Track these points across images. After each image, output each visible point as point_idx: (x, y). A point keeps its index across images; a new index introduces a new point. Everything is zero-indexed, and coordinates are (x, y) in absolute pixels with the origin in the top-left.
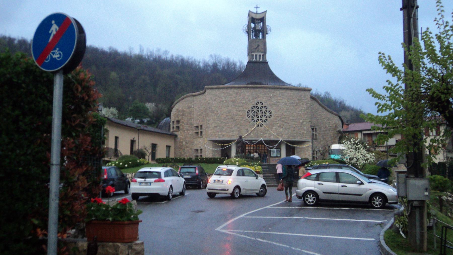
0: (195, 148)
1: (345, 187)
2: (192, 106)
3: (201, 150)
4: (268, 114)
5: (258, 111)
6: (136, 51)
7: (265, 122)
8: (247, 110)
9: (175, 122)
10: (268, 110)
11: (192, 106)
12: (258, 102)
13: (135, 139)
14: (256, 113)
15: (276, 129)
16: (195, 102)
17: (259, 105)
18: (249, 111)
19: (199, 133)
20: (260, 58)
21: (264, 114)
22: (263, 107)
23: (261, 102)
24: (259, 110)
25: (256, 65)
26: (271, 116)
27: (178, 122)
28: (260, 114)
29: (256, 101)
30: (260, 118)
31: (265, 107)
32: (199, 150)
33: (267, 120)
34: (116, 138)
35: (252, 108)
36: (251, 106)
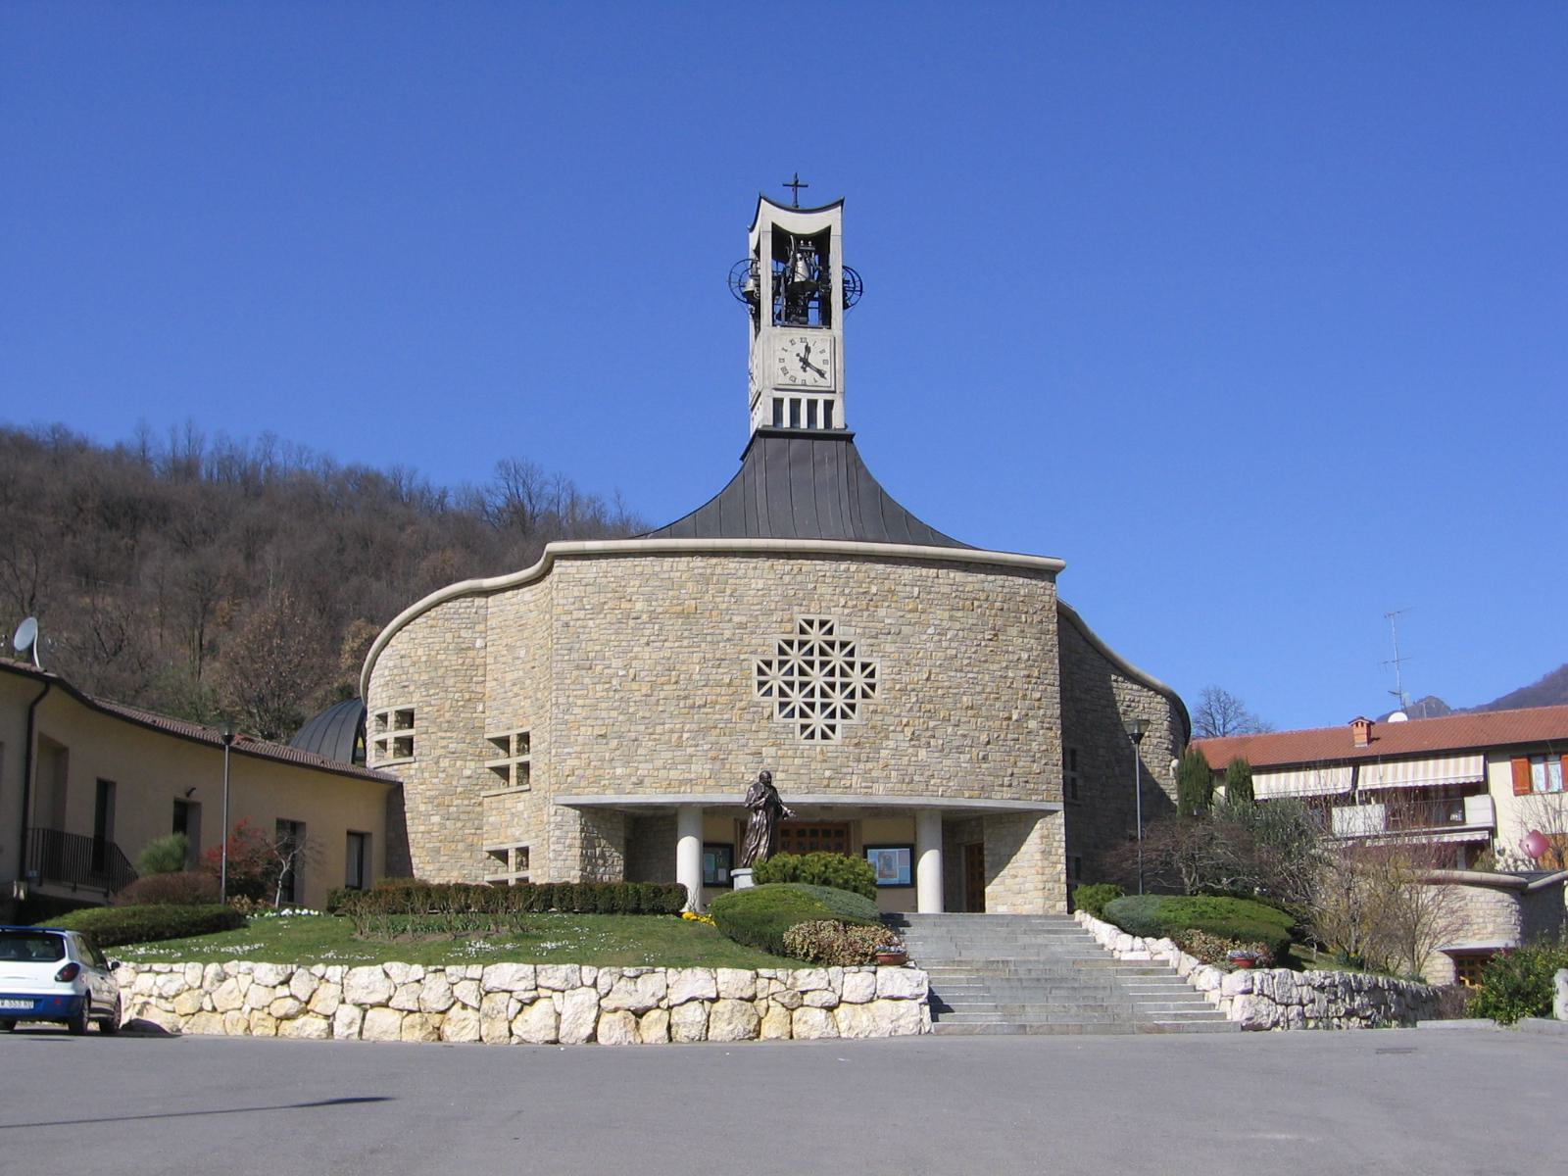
0: (490, 845)
1: (526, 1045)
2: (479, 643)
3: (524, 852)
4: (858, 680)
5: (811, 664)
6: (164, 443)
7: (844, 716)
8: (756, 662)
9: (391, 719)
10: (858, 660)
11: (479, 643)
12: (810, 623)
13: (194, 798)
14: (802, 672)
15: (897, 752)
16: (492, 623)
17: (816, 637)
18: (769, 664)
19: (513, 773)
20: (812, 419)
21: (838, 679)
22: (831, 645)
23: (823, 624)
24: (817, 658)
25: (796, 443)
26: (872, 687)
27: (407, 718)
28: (817, 678)
29: (799, 619)
30: (818, 699)
31: (843, 645)
32: (512, 854)
33: (852, 707)
34: (105, 789)
35: (782, 651)
36: (776, 640)
